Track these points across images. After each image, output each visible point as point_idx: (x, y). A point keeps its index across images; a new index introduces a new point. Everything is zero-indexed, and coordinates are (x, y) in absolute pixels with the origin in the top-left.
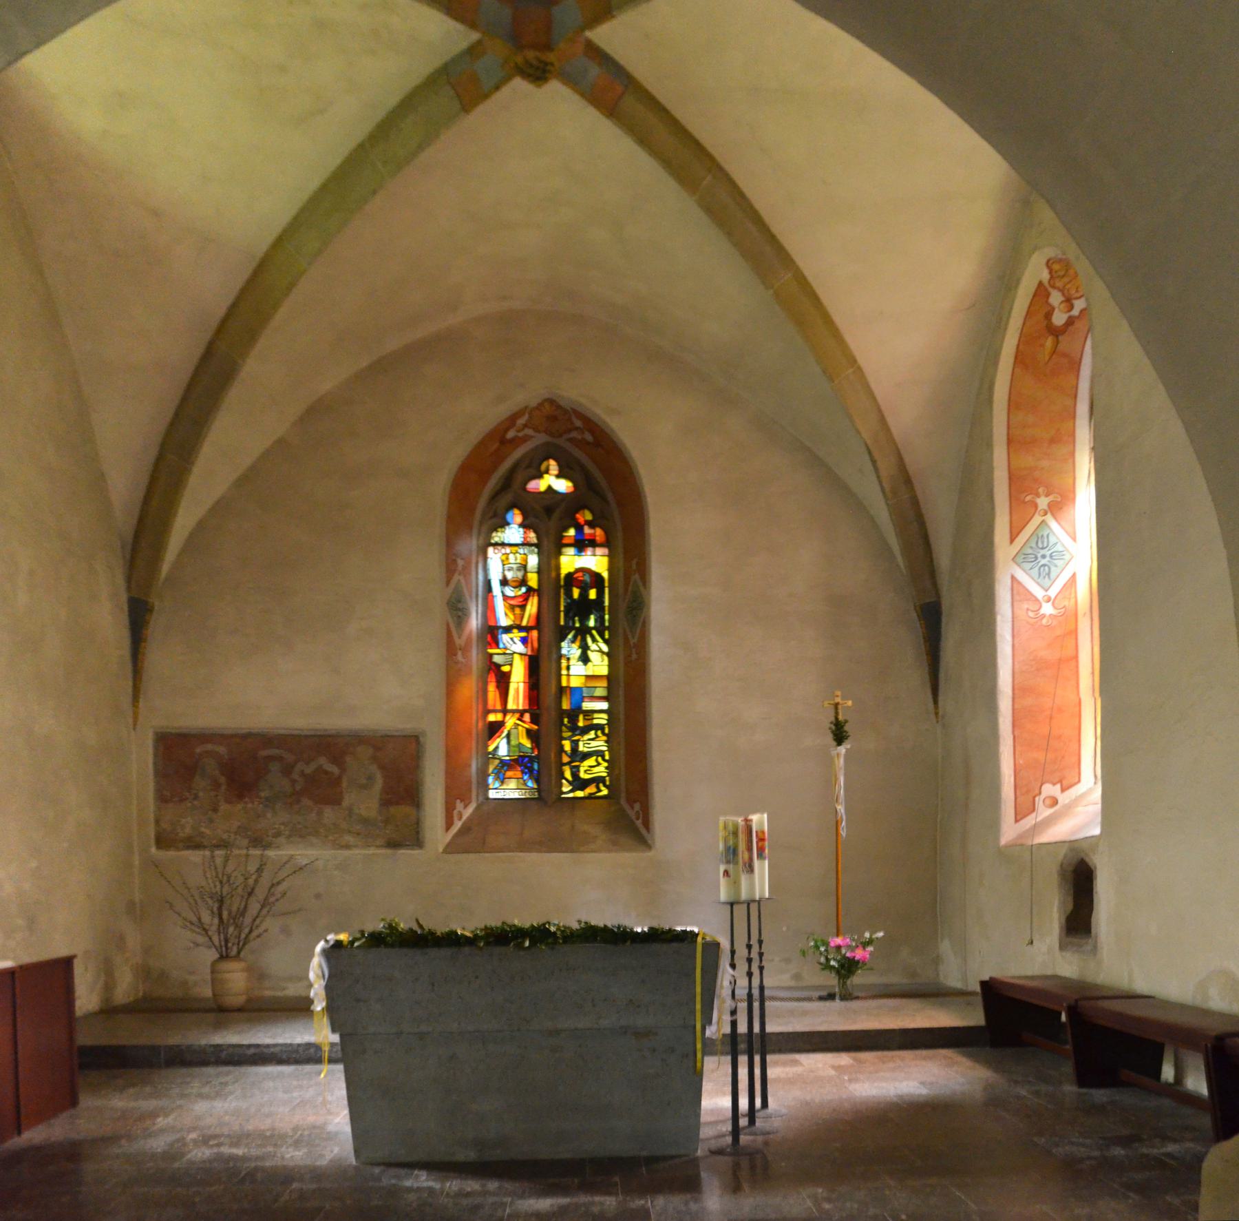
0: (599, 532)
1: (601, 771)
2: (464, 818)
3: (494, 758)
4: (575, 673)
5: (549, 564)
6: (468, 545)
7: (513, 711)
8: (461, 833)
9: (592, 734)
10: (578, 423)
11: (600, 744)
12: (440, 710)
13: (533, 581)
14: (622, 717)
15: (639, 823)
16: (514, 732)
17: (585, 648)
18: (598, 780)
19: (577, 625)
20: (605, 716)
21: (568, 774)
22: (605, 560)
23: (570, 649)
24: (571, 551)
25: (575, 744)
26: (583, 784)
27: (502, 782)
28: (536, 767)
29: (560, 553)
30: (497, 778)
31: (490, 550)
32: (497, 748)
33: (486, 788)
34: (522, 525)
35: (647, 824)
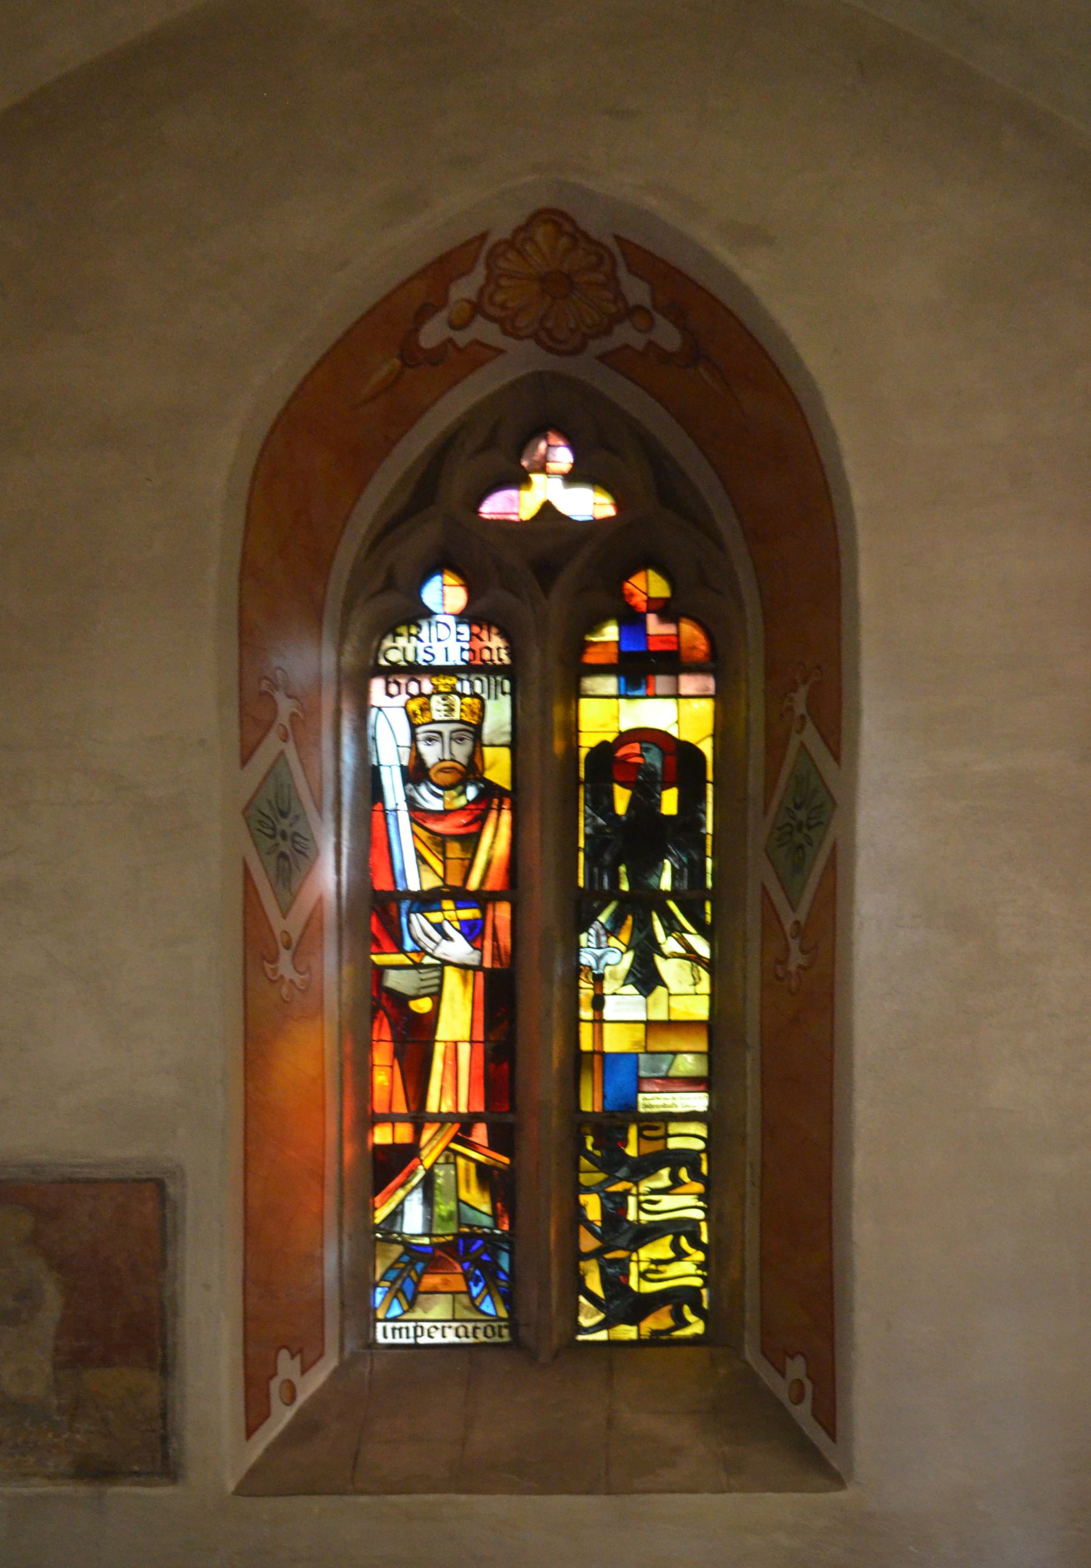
0: (689, 630)
1: (686, 1272)
2: (301, 1398)
3: (388, 1240)
4: (621, 1017)
5: (545, 714)
6: (308, 661)
7: (442, 1119)
8: (304, 1428)
9: (663, 1178)
10: (637, 292)
11: (685, 1204)
12: (225, 1105)
13: (498, 767)
14: (752, 1126)
15: (802, 1413)
16: (439, 1172)
17: (645, 953)
18: (677, 1299)
19: (625, 887)
20: (701, 1130)
21: (594, 1283)
22: (705, 708)
23: (607, 954)
24: (609, 684)
25: (614, 1207)
26: (637, 1307)
27: (412, 1305)
28: (504, 1262)
29: (578, 693)
30: (395, 1292)
31: (377, 686)
32: (397, 1213)
33: (369, 1318)
34: (462, 617)
35: (829, 1413)
